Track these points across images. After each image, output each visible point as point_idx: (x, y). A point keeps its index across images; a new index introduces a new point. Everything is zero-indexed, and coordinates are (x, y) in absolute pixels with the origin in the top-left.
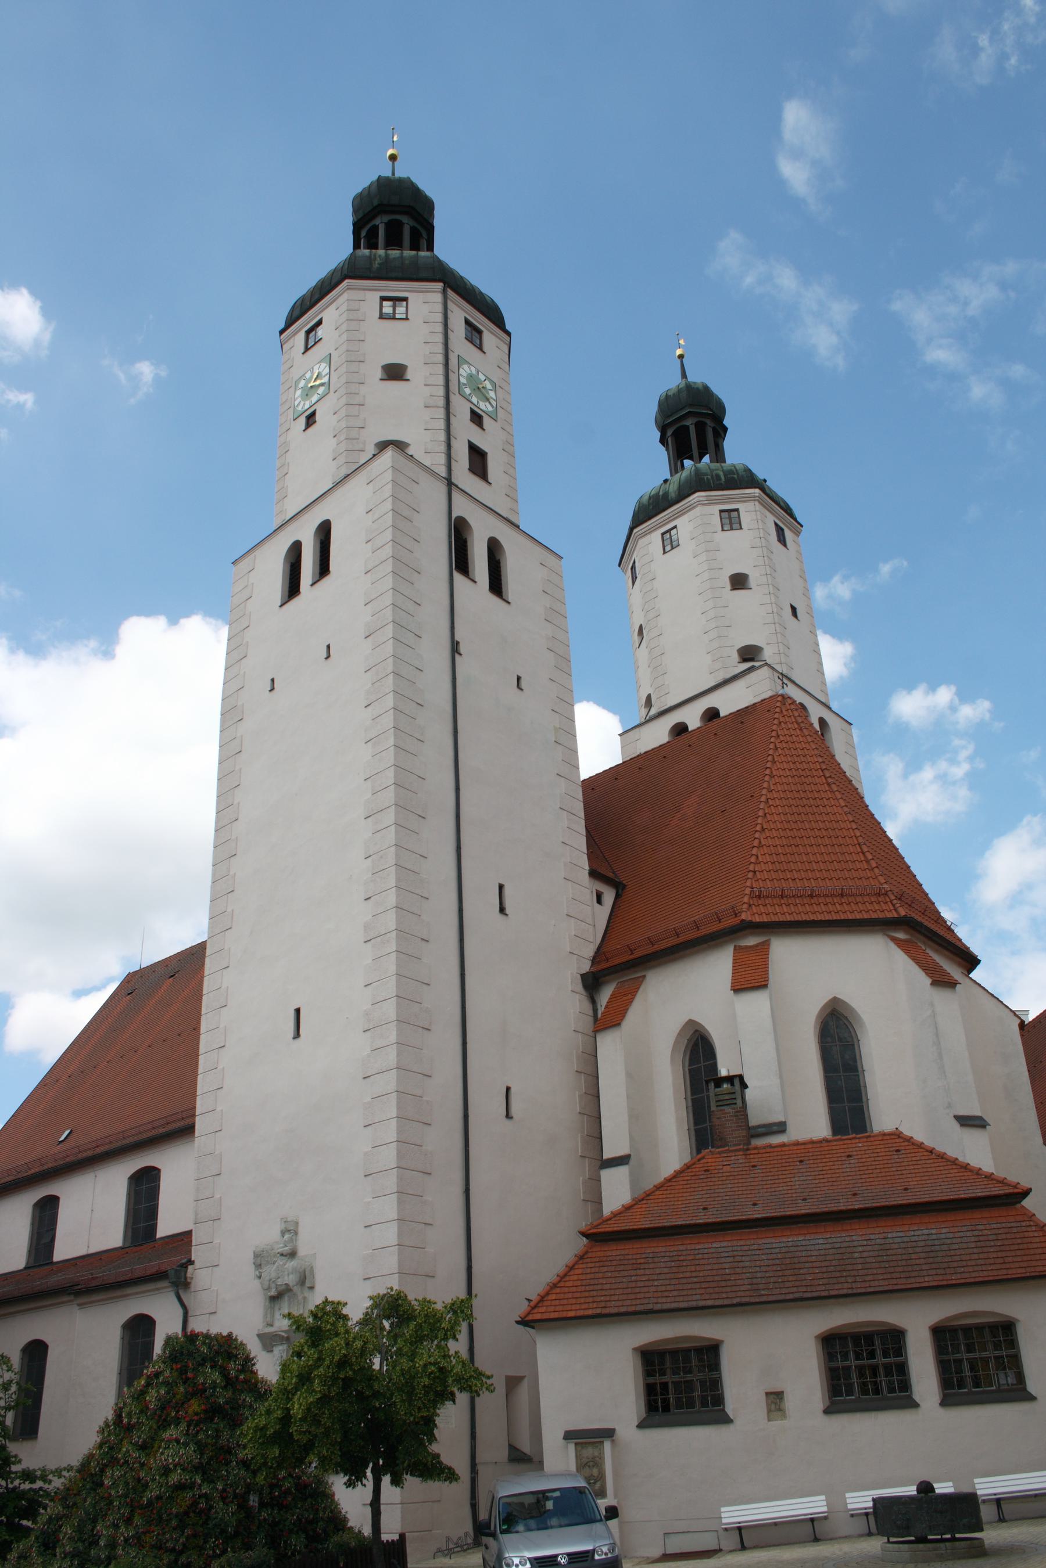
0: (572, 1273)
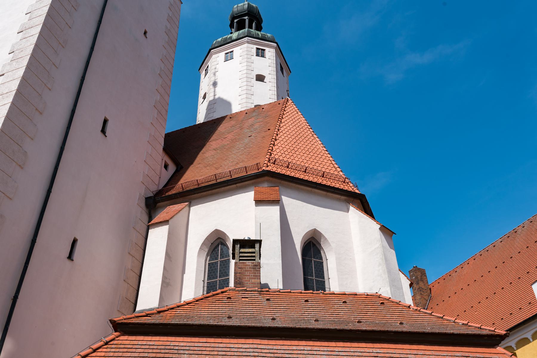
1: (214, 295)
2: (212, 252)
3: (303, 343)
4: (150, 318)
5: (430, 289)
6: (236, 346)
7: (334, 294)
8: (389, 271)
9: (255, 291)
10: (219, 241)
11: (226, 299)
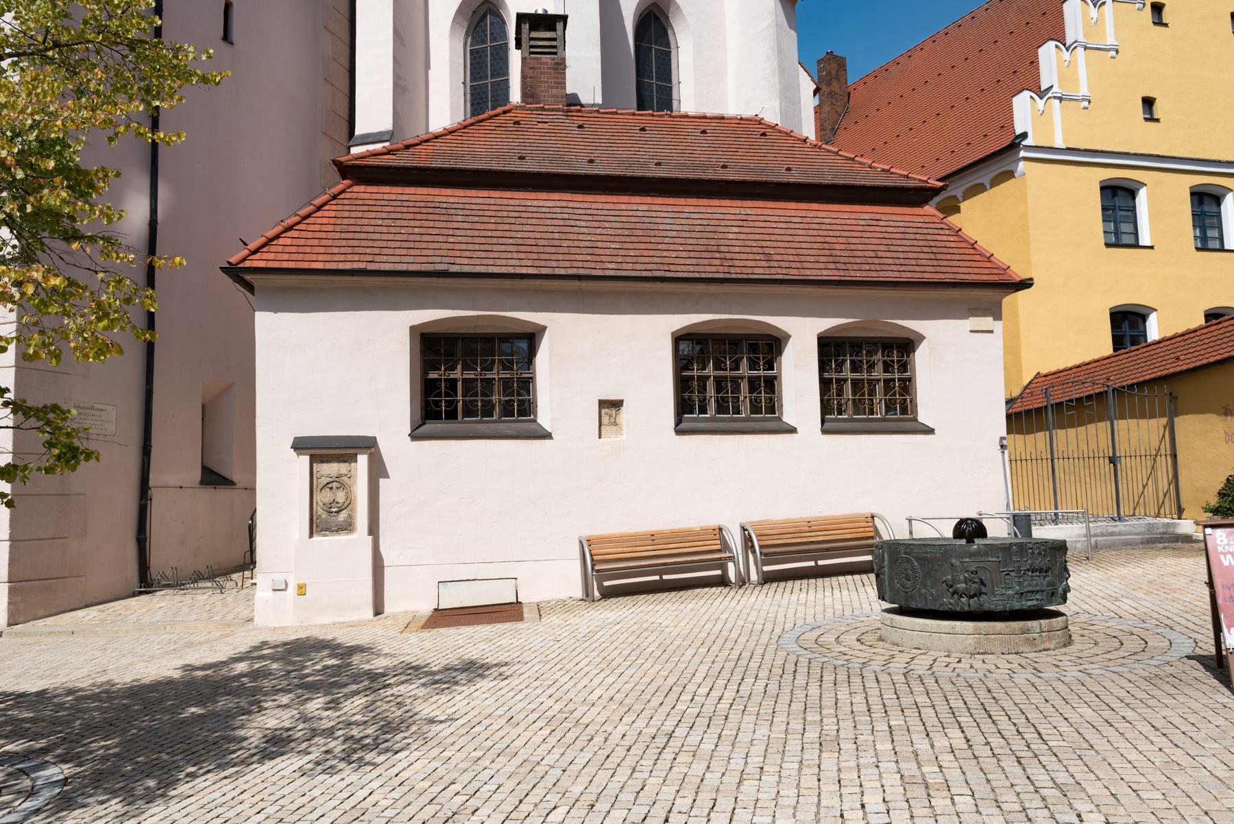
0: (319, 214)
1: (491, 117)
2: (475, 28)
3: (637, 199)
4: (394, 157)
5: (849, 94)
6: (536, 203)
7: (687, 116)
8: (783, 71)
9: (558, 110)
10: (486, 6)
11: (512, 125)
